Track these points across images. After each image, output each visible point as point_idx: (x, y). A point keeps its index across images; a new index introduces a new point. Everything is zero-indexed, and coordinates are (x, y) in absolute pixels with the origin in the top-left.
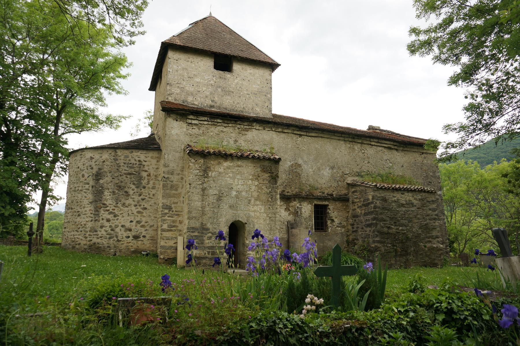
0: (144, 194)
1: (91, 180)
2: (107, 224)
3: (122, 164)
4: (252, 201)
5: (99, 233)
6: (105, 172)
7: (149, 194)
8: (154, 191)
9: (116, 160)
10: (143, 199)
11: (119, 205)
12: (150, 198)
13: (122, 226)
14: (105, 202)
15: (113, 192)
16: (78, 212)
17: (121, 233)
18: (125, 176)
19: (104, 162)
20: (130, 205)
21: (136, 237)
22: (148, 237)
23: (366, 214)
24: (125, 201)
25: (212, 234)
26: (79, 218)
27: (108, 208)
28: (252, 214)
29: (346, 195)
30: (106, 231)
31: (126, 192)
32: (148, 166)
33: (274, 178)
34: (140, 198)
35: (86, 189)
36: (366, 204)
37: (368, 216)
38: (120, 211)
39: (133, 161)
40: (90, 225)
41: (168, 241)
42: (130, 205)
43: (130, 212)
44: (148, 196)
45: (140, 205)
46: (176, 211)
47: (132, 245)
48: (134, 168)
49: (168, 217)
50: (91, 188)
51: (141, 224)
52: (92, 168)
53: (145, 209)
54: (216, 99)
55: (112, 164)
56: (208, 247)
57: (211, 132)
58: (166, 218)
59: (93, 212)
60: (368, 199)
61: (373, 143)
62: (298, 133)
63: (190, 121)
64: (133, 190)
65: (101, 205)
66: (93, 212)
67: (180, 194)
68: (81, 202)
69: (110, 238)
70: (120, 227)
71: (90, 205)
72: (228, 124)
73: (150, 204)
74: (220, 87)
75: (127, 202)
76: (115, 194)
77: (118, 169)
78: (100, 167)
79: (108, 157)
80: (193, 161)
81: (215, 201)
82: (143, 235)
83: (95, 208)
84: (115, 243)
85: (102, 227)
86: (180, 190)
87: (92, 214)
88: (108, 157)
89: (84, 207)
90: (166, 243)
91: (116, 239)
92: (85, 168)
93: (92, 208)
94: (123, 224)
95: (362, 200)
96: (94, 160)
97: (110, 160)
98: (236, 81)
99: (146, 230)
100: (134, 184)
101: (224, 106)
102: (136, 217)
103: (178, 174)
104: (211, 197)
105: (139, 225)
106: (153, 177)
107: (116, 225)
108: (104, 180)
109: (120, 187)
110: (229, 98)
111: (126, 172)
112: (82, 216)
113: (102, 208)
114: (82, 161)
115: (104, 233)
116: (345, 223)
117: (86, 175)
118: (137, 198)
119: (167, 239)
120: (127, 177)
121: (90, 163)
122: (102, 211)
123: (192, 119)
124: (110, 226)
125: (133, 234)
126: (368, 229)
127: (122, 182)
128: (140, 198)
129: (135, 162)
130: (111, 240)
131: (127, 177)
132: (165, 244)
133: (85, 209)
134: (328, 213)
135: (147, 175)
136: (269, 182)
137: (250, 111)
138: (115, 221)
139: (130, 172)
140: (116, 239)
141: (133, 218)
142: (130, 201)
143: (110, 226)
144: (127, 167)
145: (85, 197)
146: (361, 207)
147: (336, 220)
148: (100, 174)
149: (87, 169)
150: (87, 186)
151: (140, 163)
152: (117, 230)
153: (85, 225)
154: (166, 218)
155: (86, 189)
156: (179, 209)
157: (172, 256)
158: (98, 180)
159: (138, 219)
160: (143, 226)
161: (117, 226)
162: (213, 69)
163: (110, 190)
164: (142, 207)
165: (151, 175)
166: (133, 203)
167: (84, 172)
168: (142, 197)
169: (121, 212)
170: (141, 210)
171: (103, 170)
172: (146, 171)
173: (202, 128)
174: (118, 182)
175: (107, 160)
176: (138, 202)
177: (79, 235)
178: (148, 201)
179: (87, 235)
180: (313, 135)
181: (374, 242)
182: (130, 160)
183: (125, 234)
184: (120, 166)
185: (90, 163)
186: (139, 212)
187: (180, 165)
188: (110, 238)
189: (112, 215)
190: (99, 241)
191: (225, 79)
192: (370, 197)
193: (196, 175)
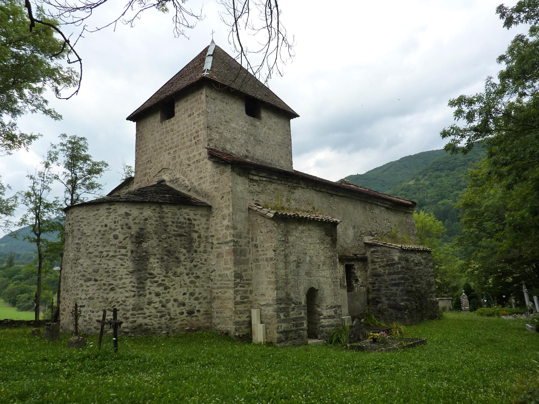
0: (196, 260)
1: (129, 242)
2: (156, 299)
3: (170, 223)
4: (321, 266)
5: (145, 311)
6: (149, 233)
7: (201, 260)
8: (205, 256)
9: (161, 218)
10: (195, 266)
11: (170, 274)
12: (202, 263)
13: (175, 300)
14: (152, 271)
15: (162, 258)
16: (110, 284)
17: (174, 309)
18: (174, 238)
19: (146, 219)
20: (181, 274)
21: (190, 313)
22: (202, 310)
23: (389, 274)
24: (176, 270)
25: (295, 304)
27: (156, 279)
28: (322, 279)
29: (364, 254)
30: (156, 308)
31: (177, 258)
32: (198, 225)
33: (334, 241)
34: (192, 264)
35: (122, 255)
36: (391, 264)
37: (394, 276)
38: (171, 282)
39: (182, 220)
40: (131, 302)
41: (241, 315)
42: (181, 274)
43: (182, 282)
44: (200, 262)
45: (193, 274)
46: (246, 280)
47: (186, 322)
48: (183, 228)
49: (241, 287)
50: (129, 254)
51: (195, 296)
52: (130, 228)
53: (198, 277)
54: (249, 148)
55: (157, 223)
56: (293, 319)
57: (269, 189)
58: (239, 288)
59: (136, 285)
60: (393, 260)
61: (379, 204)
62: (330, 192)
63: (251, 177)
64: (184, 255)
65: (147, 275)
66: (136, 285)
67: (248, 259)
68: (115, 272)
69: (161, 317)
70: (172, 302)
71: (130, 276)
72: (281, 181)
73: (202, 271)
74: (252, 135)
75: (179, 270)
76: (164, 261)
77: (165, 230)
78: (142, 226)
79: (152, 214)
80: (276, 225)
81: (295, 268)
82: (197, 309)
83: (138, 279)
84: (168, 323)
85: (149, 303)
86: (248, 256)
87: (134, 287)
88: (152, 214)
89: (121, 279)
90: (239, 317)
91: (168, 317)
92: (119, 227)
93: (133, 279)
94: (175, 297)
95: (385, 260)
96: (131, 218)
97: (154, 218)
98: (264, 129)
99: (200, 303)
100: (185, 248)
101: (256, 157)
102: (189, 288)
103: (246, 237)
104: (292, 264)
105: (192, 298)
106: (204, 239)
107: (167, 300)
108: (149, 243)
109: (169, 251)
110: (260, 148)
111: (175, 233)
112: (118, 290)
113: (149, 280)
114: (110, 217)
115: (154, 311)
116: (365, 283)
117: (121, 237)
118: (189, 265)
119: (241, 313)
120: (176, 240)
121: (126, 221)
122: (148, 283)
123: (253, 175)
124: (161, 302)
125: (187, 309)
126: (394, 288)
127: (171, 246)
128: (192, 264)
129: (185, 221)
130: (163, 319)
131: (176, 240)
132: (239, 319)
133: (123, 281)
134: (354, 273)
135: (198, 237)
136: (331, 245)
137: (277, 164)
138: (167, 294)
139: (179, 232)
140: (168, 317)
141: (186, 289)
142: (181, 269)
143: (161, 302)
144: (177, 226)
145: (122, 265)
146: (383, 266)
147: (360, 279)
148: (142, 235)
149: (122, 229)
150: (123, 251)
151: (190, 222)
152: (169, 305)
153: (124, 302)
154: (239, 288)
155: (122, 255)
156: (249, 277)
157: (244, 330)
158: (140, 243)
159: (191, 290)
160: (196, 299)
161: (168, 301)
162: (245, 115)
163: (158, 256)
164: (195, 275)
165: (202, 236)
166: (185, 271)
167: (116, 233)
168: (194, 263)
169: (171, 284)
170: (194, 279)
171: (146, 231)
172: (196, 232)
173: (262, 185)
174: (166, 245)
175: (151, 218)
176: (191, 269)
178: (200, 268)
179: (128, 315)
180: (341, 194)
181: (403, 300)
182: (178, 218)
183: (178, 310)
184: (167, 226)
185: (126, 221)
186: (191, 282)
187: (246, 227)
188: (161, 317)
189: (161, 288)
190: (147, 321)
191: (255, 126)
192: (396, 258)
193: (279, 241)
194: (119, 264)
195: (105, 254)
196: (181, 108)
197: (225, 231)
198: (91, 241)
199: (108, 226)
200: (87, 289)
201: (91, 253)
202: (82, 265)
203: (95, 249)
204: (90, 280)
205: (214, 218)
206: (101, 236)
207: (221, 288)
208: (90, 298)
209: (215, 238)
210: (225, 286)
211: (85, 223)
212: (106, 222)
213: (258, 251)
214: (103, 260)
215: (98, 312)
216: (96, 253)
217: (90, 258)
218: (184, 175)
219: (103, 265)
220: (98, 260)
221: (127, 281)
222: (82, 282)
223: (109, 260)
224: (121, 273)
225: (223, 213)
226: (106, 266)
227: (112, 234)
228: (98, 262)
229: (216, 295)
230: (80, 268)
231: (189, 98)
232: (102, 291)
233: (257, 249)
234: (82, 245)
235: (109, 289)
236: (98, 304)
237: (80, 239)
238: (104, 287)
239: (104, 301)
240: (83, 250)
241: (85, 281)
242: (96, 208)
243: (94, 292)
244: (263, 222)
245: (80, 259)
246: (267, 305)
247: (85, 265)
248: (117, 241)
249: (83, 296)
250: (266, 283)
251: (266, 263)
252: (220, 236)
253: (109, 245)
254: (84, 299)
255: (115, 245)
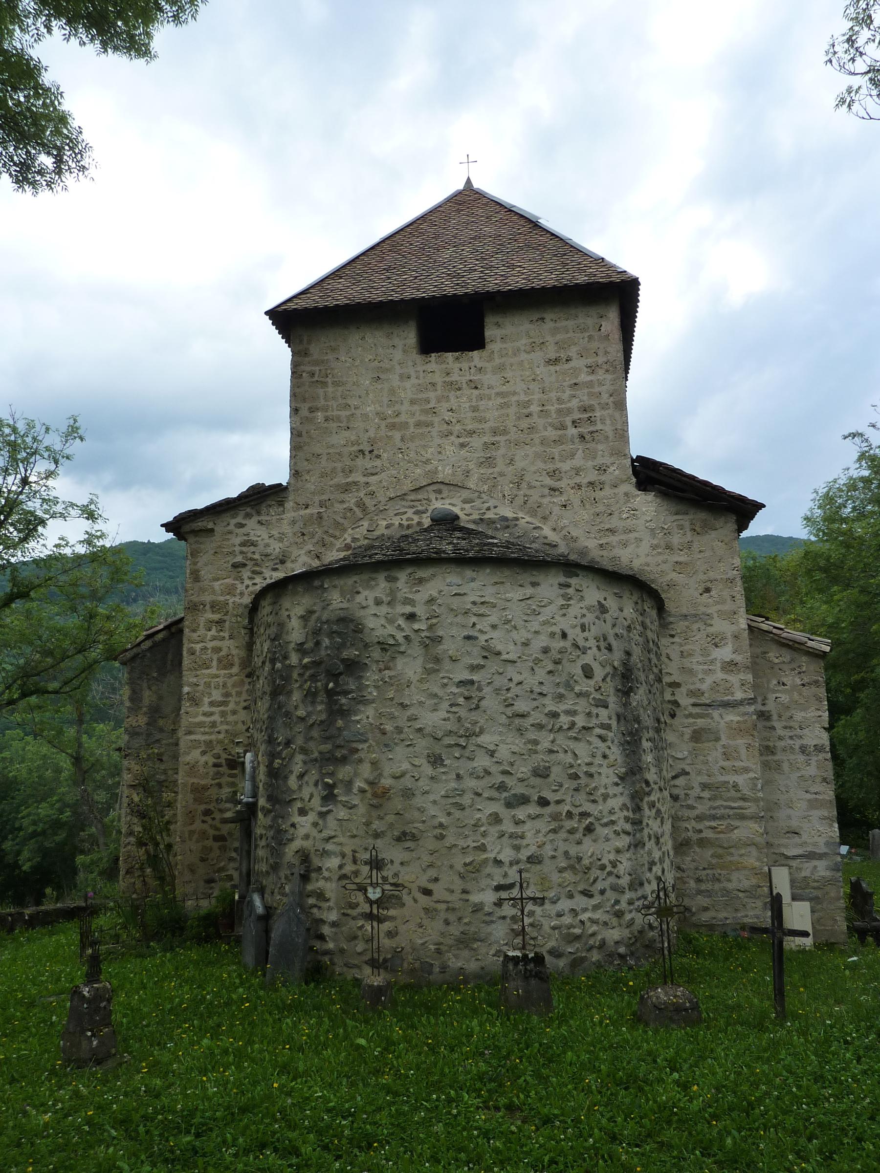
16: (584, 815)
26: (587, 841)
68: (591, 776)
89: (605, 797)
117: (599, 673)
150: (603, 713)
153: (614, 864)
167: (588, 659)
177: (596, 908)
194: (599, 754)
195: (564, 720)
196: (505, 335)
197: (720, 675)
198: (517, 678)
199: (570, 637)
200: (519, 830)
201: (523, 716)
202: (492, 754)
203: (535, 703)
204: (524, 800)
205: (676, 639)
206: (550, 667)
207: (714, 818)
208: (531, 860)
209: (683, 690)
210: (731, 812)
211: (494, 619)
212: (564, 624)
213: (773, 728)
214: (561, 739)
215: (554, 903)
216: (537, 717)
217: (520, 731)
218: (533, 513)
219: (561, 756)
220: (545, 740)
221: (615, 803)
222: (497, 807)
223: (576, 739)
224: (604, 780)
225: (710, 630)
226: (569, 758)
227: (580, 663)
228: (545, 744)
229: (695, 837)
230: (482, 762)
231: (549, 316)
232: (563, 835)
233: (768, 724)
234: (487, 690)
235: (581, 830)
236: (555, 877)
237: (474, 668)
238: (569, 824)
239: (572, 868)
240: (491, 703)
241: (509, 805)
242: (526, 577)
243: (541, 838)
244: (787, 659)
245: (481, 732)
246: (811, 856)
247: (503, 753)
248: (592, 682)
249: (506, 855)
250: (803, 805)
251: (801, 758)
252: (704, 687)
253: (573, 695)
254: (511, 864)
255: (586, 695)
